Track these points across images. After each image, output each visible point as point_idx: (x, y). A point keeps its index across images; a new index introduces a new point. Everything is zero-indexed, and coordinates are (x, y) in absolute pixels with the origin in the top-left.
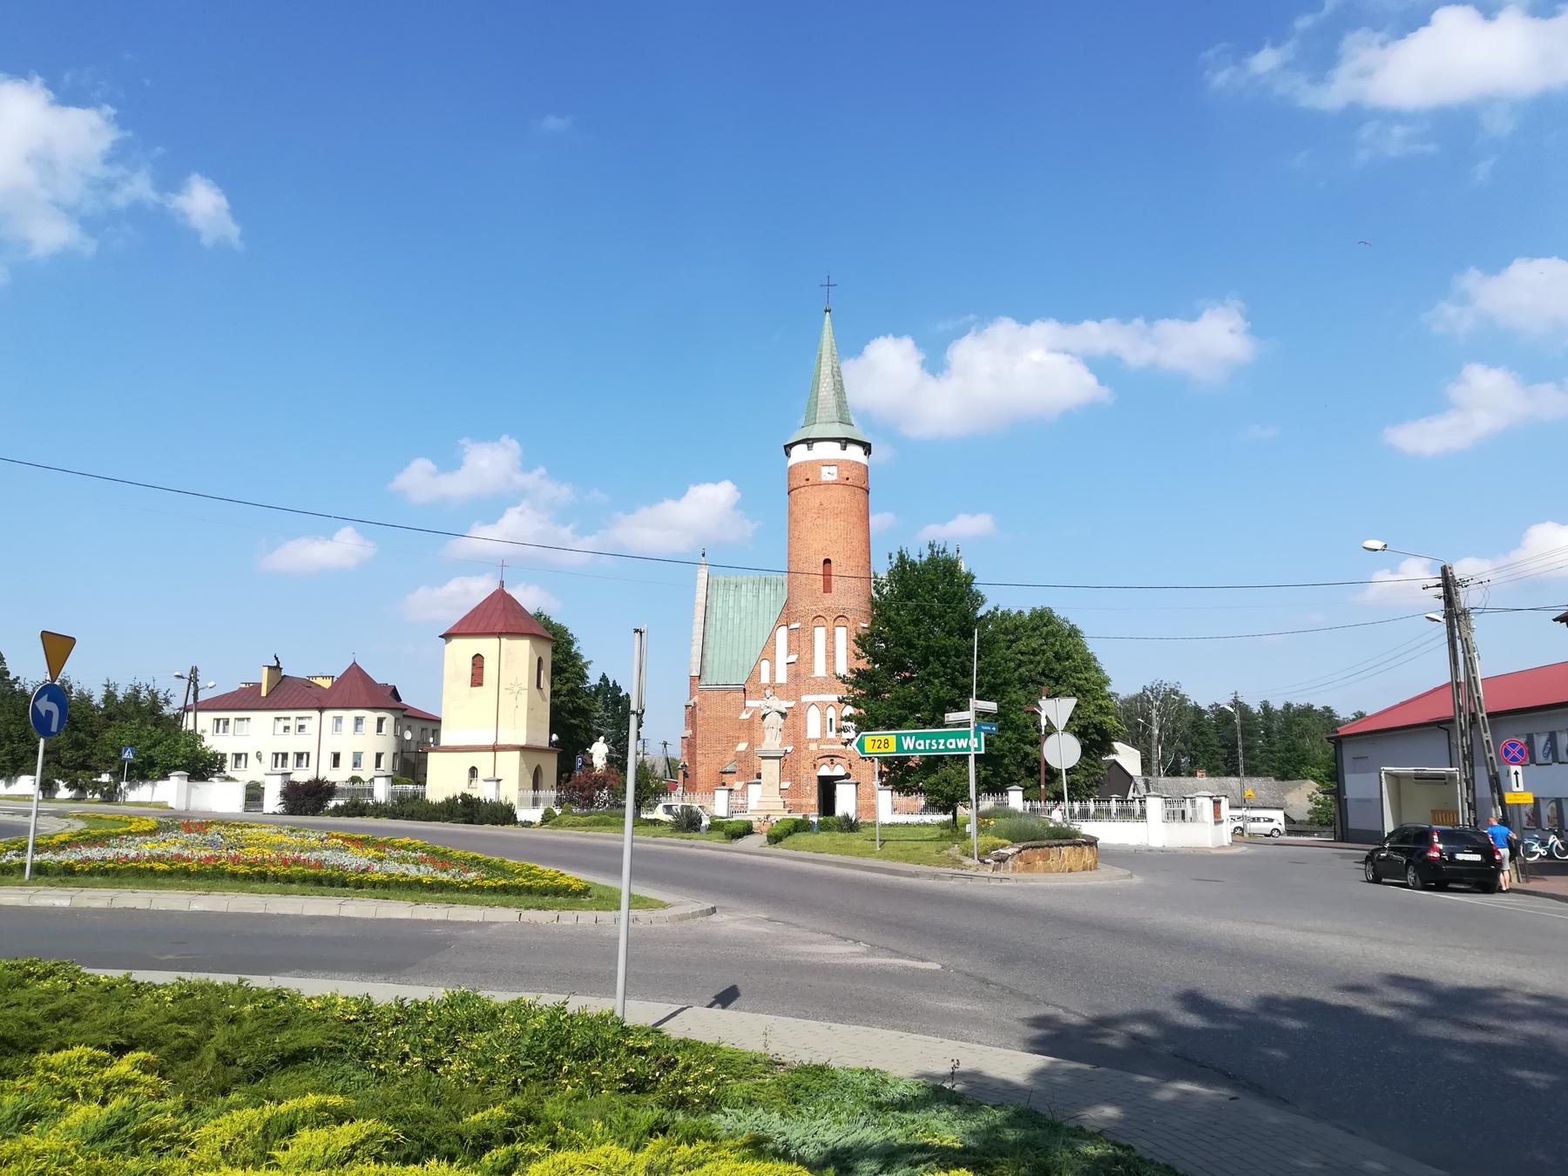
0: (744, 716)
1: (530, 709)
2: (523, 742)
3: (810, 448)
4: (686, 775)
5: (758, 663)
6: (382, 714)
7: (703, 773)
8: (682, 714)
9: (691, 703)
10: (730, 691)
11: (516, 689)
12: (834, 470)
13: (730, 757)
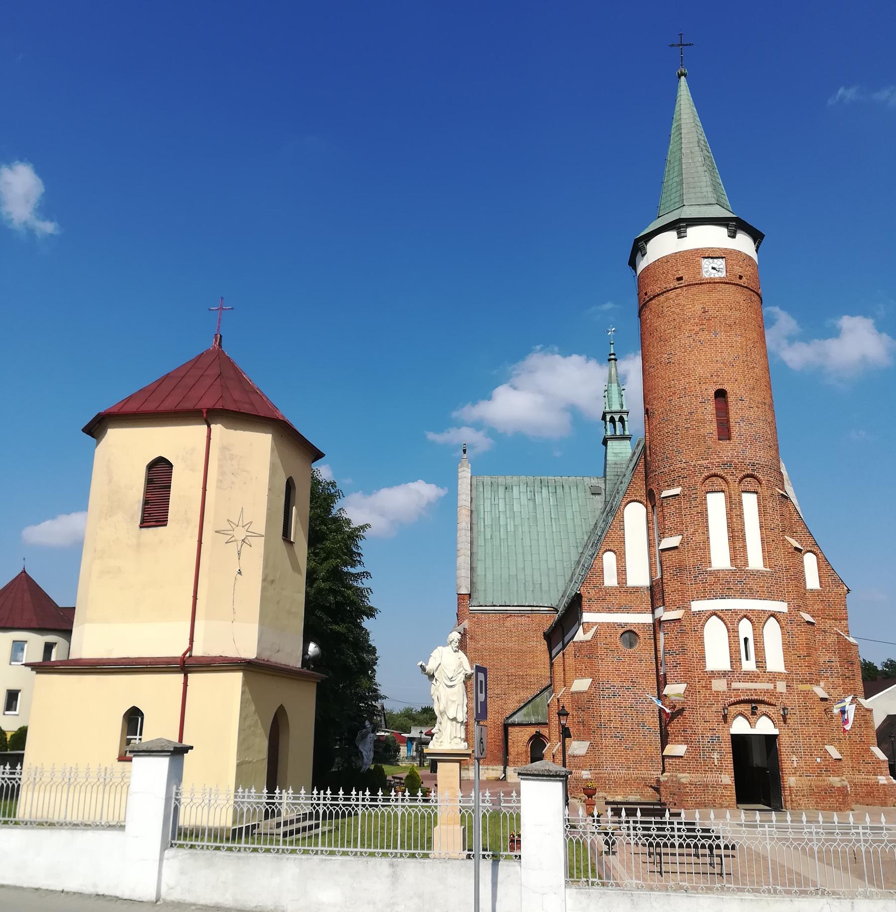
1: (268, 581)
2: (250, 652)
6: (51, 638)
10: (510, 615)
11: (240, 534)
12: (720, 263)
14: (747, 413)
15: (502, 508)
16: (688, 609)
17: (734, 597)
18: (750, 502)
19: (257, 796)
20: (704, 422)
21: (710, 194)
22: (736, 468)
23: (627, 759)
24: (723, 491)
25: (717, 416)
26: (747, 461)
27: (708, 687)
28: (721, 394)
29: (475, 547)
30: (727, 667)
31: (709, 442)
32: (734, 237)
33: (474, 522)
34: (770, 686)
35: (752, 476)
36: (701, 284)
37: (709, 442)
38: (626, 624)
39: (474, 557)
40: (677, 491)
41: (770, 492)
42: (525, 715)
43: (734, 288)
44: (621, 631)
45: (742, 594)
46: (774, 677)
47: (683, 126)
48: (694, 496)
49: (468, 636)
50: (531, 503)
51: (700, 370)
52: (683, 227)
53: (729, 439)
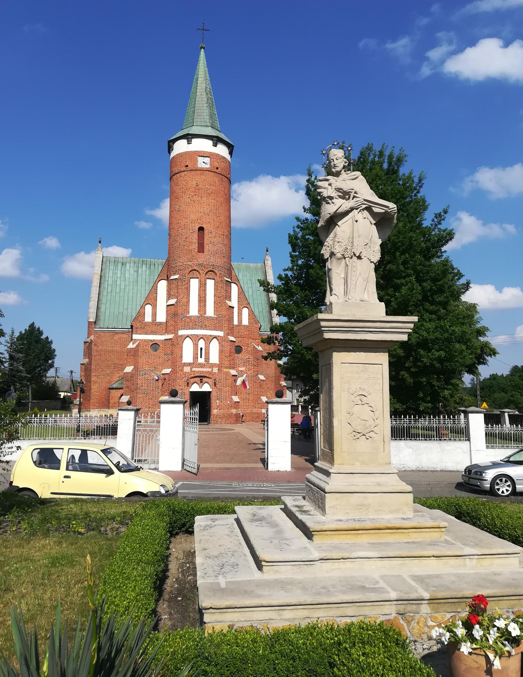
0: (131, 346)
3: (189, 143)
4: (82, 391)
5: (143, 307)
7: (96, 389)
8: (81, 347)
9: (88, 340)
12: (207, 160)
13: (116, 378)
14: (213, 240)
15: (119, 275)
16: (176, 334)
17: (198, 329)
18: (210, 284)
20: (191, 243)
21: (208, 121)
22: (204, 267)
23: (149, 404)
25: (198, 240)
26: (211, 264)
27: (182, 370)
28: (201, 229)
29: (101, 296)
31: (194, 253)
32: (216, 146)
33: (102, 282)
34: (210, 370)
35: (212, 271)
37: (194, 253)
38: (154, 340)
39: (100, 302)
40: (177, 277)
41: (220, 279)
42: (119, 384)
44: (151, 343)
45: (201, 328)
46: (213, 366)
50: (136, 273)
51: (192, 216)
52: (190, 138)
53: (203, 252)
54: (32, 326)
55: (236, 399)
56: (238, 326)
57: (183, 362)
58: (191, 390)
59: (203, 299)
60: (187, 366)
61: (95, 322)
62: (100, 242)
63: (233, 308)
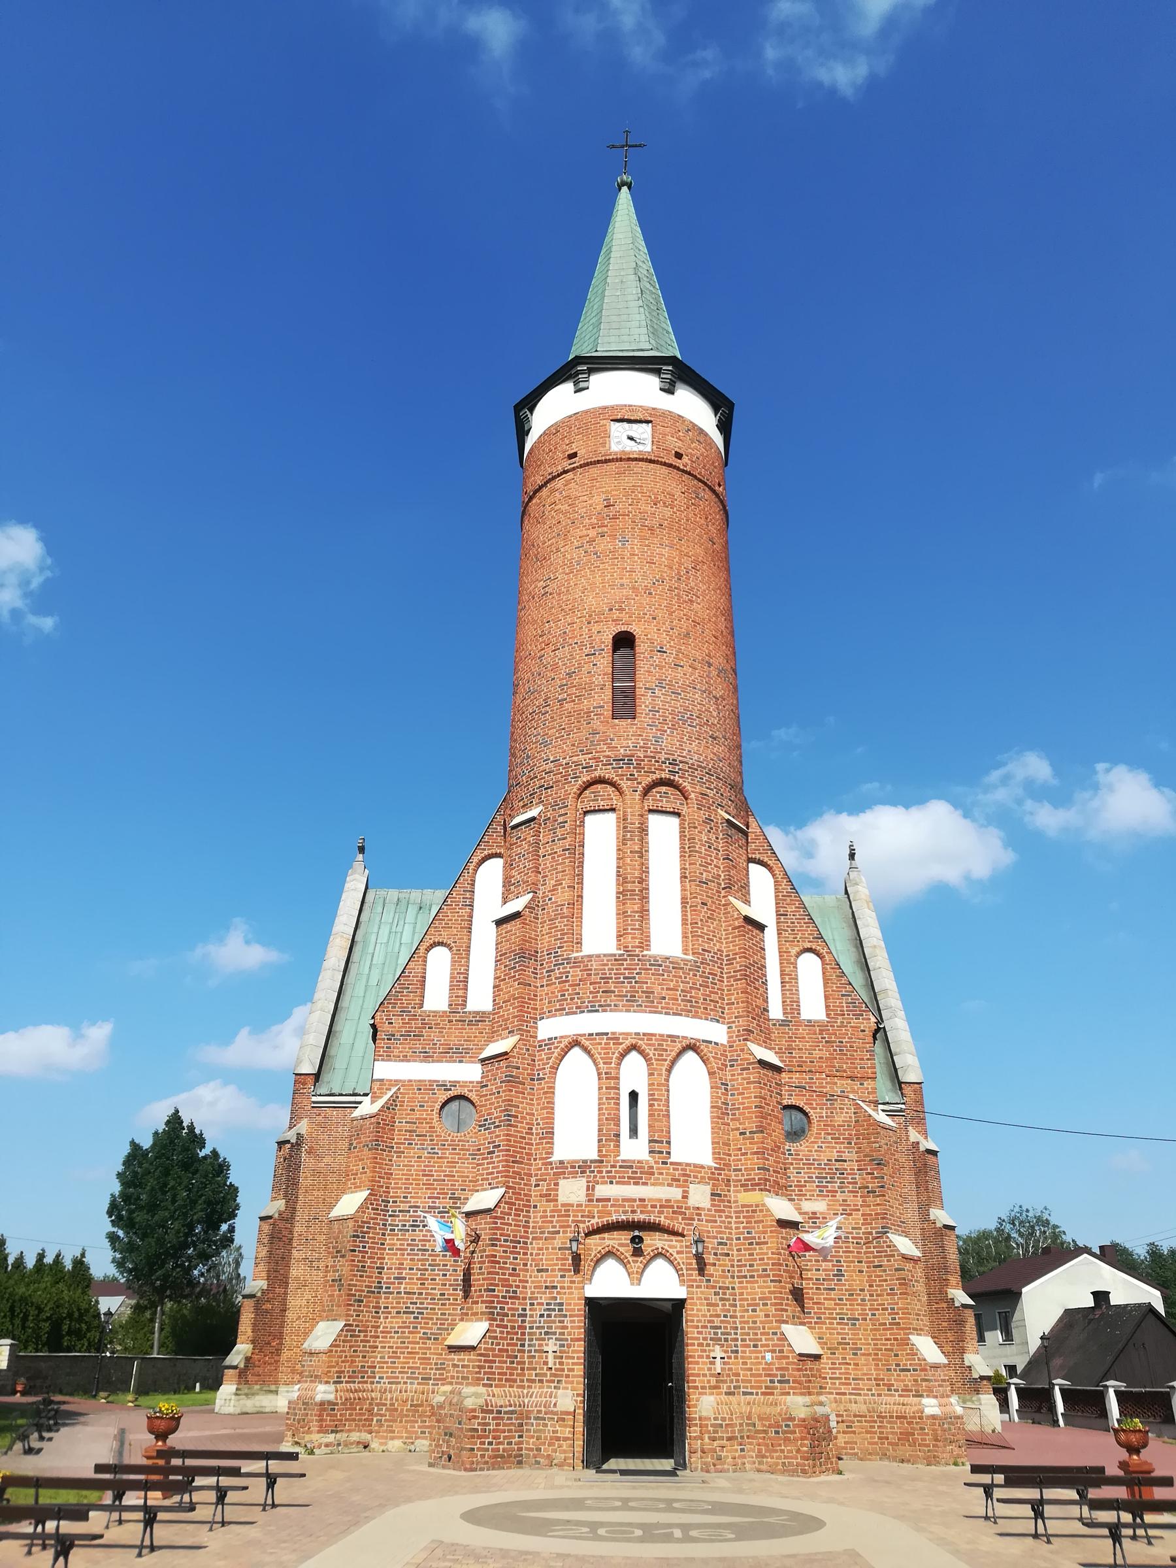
5: (418, 956)
9: (291, 1136)
12: (643, 432)
14: (669, 674)
17: (616, 1008)
18: (664, 833)
19: (325, 1468)
21: (644, 338)
22: (639, 767)
24: (613, 810)
26: (663, 757)
27: (550, 1197)
28: (624, 641)
30: (590, 1152)
34: (675, 1193)
36: (607, 461)
37: (596, 724)
38: (454, 1084)
41: (703, 815)
43: (664, 470)
44: (443, 1097)
45: (631, 1003)
46: (685, 1175)
47: (613, 249)
48: (560, 819)
49: (305, 1147)
51: (591, 601)
52: (582, 372)
54: (175, 1120)
55: (802, 1339)
56: (784, 1023)
57: (556, 1158)
58: (592, 1291)
59: (637, 887)
60: (574, 1174)
61: (317, 1077)
62: (362, 850)
63: (761, 927)
